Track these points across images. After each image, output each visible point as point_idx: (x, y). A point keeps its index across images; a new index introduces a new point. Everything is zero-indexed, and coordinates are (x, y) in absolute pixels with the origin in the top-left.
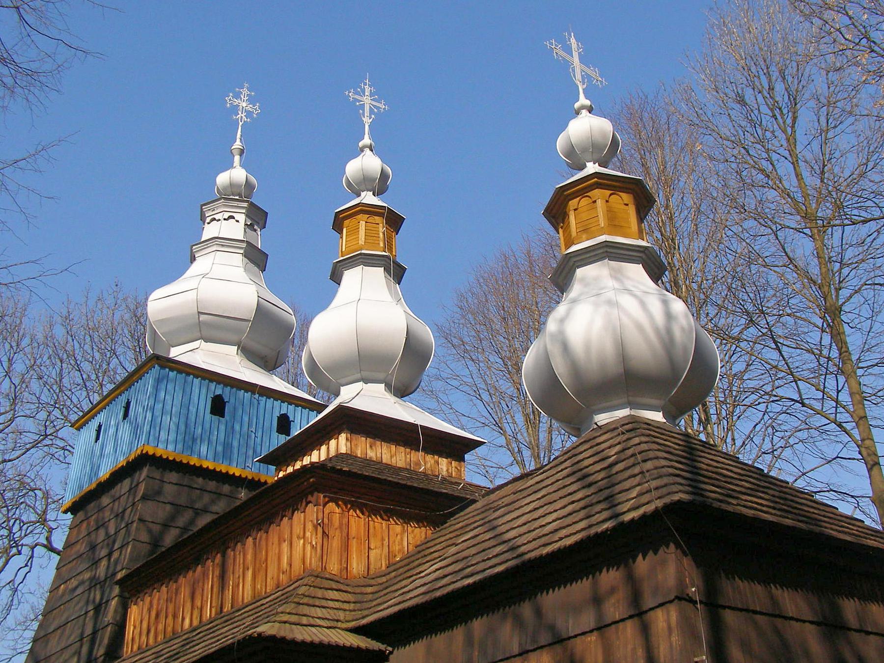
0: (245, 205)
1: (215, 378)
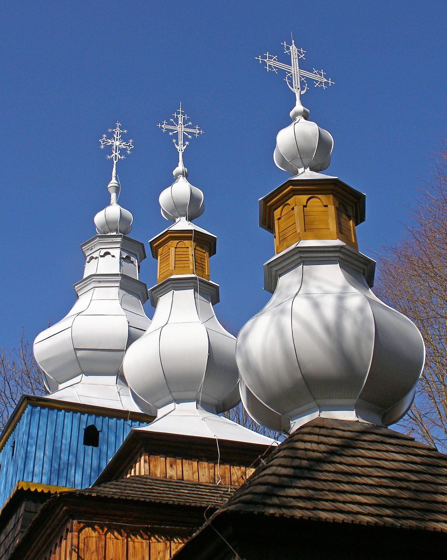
0: (119, 240)
1: (85, 410)
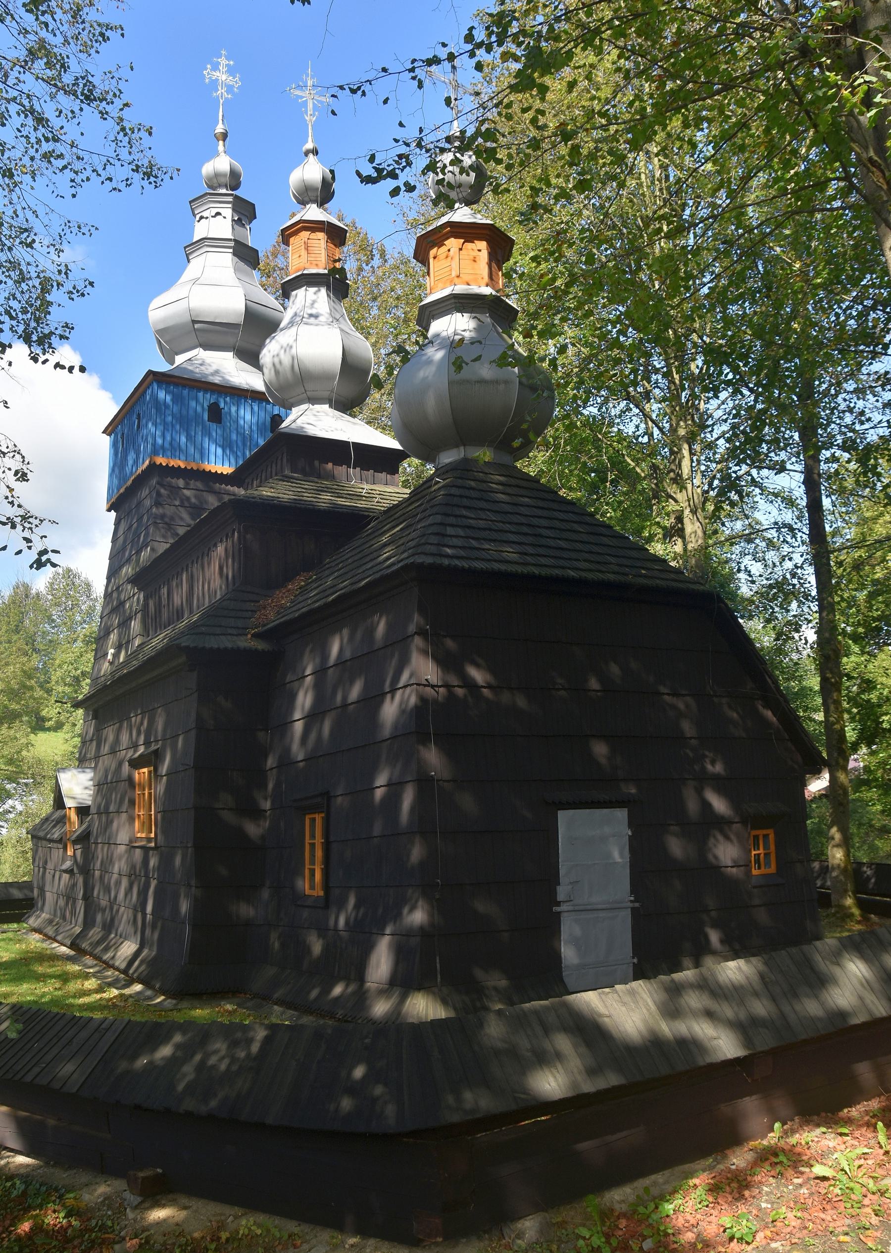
0: (230, 199)
